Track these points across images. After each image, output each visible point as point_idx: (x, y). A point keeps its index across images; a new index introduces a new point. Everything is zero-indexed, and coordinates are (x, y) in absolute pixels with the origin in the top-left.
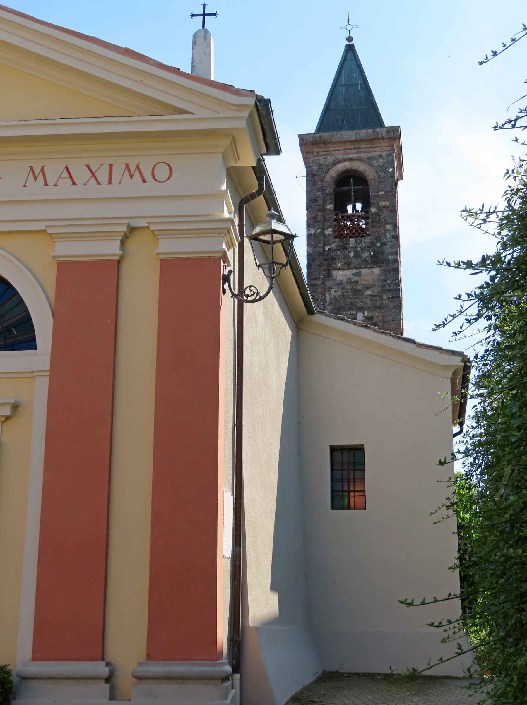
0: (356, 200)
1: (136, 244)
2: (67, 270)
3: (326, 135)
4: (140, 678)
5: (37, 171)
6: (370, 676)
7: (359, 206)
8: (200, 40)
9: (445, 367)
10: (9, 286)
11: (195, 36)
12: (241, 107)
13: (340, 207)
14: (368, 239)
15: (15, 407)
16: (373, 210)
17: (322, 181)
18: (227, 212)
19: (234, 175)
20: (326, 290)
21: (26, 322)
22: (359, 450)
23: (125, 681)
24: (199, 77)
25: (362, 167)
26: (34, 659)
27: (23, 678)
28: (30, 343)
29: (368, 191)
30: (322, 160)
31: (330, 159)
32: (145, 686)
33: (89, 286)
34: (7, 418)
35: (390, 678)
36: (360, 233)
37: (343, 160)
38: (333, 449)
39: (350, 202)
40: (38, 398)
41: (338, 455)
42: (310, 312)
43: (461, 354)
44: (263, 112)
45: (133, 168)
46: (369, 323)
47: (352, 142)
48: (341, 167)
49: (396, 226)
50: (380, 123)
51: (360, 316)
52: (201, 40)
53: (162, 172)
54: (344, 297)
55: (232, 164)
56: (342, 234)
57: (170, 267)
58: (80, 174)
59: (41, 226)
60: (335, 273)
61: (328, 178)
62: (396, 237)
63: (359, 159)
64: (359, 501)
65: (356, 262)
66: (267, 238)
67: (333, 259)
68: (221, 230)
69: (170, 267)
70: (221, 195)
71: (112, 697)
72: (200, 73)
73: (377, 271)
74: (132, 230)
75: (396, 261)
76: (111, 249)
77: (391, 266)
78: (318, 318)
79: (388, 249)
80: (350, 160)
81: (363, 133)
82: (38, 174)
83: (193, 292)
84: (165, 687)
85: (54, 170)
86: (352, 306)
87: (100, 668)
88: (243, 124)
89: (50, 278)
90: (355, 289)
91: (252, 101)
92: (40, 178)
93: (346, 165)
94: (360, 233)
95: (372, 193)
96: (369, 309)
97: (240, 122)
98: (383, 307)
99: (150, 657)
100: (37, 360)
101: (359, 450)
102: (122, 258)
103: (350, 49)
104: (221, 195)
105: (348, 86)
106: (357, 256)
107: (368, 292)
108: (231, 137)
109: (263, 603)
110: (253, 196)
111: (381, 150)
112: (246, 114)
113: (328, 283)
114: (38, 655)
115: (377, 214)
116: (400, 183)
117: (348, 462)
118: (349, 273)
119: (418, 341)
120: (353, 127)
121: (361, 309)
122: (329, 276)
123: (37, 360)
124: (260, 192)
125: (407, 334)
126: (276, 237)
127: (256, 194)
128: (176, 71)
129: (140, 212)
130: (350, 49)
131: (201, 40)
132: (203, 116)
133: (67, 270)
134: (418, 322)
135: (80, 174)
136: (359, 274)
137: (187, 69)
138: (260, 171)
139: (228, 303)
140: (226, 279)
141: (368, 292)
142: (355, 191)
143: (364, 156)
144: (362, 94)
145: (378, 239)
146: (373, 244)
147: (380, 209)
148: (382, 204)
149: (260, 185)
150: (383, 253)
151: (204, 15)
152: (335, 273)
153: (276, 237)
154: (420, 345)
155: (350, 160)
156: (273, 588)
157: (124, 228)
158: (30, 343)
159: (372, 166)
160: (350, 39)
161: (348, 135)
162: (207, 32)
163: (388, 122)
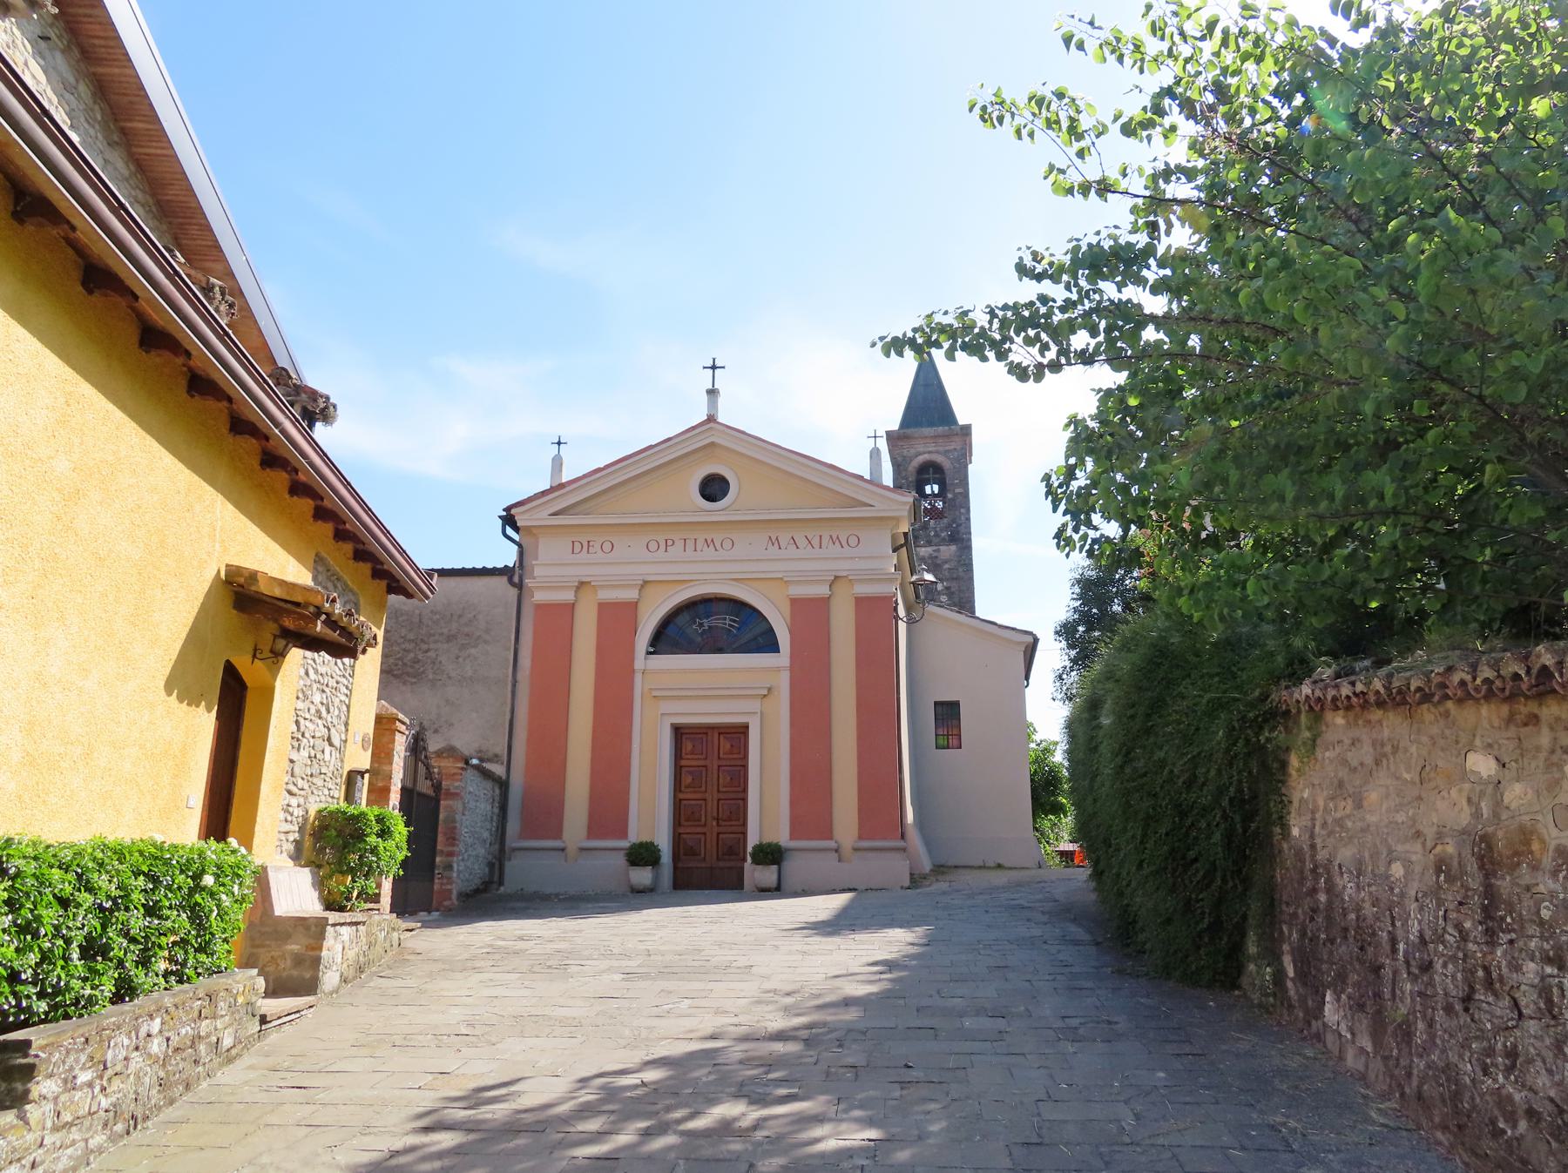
3: (909, 431)
4: (856, 849)
7: (936, 488)
15: (769, 689)
25: (939, 459)
30: (905, 452)
31: (913, 451)
32: (859, 854)
37: (924, 451)
38: (936, 703)
40: (783, 683)
43: (1030, 633)
48: (921, 459)
50: (955, 421)
53: (853, 541)
57: (862, 603)
58: (802, 542)
62: (968, 519)
65: (935, 540)
69: (862, 603)
73: (953, 548)
76: (823, 590)
79: (962, 529)
84: (871, 854)
85: (784, 539)
88: (906, 514)
93: (926, 457)
99: (860, 838)
100: (783, 658)
105: (926, 386)
106: (937, 535)
108: (897, 520)
111: (955, 444)
114: (793, 836)
117: (948, 713)
118: (930, 549)
120: (931, 424)
123: (783, 658)
128: (861, 478)
129: (843, 567)
133: (795, 602)
135: (802, 542)
137: (867, 477)
145: (954, 521)
146: (950, 525)
147: (956, 495)
154: (1001, 626)
161: (927, 431)
163: (962, 421)
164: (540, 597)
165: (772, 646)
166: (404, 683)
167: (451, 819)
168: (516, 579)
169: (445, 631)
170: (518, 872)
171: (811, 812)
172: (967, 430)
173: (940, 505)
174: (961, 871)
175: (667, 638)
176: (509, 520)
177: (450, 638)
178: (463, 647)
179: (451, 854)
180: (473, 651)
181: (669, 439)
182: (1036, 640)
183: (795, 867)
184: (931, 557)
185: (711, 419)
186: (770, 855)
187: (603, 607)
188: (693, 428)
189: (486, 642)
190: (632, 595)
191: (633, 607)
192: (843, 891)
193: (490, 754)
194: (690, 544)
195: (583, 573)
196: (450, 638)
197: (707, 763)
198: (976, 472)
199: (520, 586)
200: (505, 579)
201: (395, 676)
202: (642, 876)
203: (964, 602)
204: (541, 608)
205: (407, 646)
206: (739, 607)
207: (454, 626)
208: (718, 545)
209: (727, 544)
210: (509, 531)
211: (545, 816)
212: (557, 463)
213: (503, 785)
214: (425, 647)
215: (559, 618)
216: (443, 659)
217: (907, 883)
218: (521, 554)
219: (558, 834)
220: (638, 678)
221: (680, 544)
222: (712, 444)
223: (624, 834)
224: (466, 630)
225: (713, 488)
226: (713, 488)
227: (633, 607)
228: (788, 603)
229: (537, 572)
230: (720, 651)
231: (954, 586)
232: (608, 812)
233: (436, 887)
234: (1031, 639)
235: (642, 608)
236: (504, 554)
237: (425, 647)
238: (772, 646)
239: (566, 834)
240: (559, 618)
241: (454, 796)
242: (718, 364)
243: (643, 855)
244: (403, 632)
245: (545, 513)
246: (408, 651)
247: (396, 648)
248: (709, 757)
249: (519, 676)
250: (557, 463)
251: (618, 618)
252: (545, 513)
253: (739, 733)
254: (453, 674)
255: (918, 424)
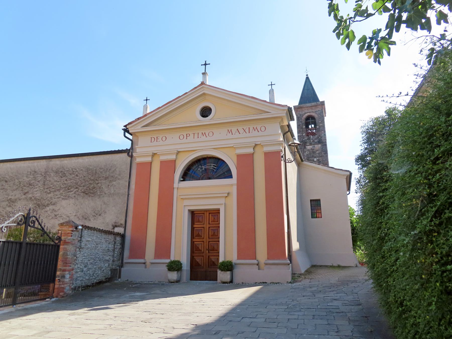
0: (312, 124)
1: (257, 149)
2: (239, 157)
3: (301, 105)
4: (266, 264)
5: (230, 131)
6: (326, 266)
7: (313, 126)
8: (271, 92)
9: (344, 175)
10: (224, 161)
11: (270, 91)
12: (284, 110)
13: (307, 127)
14: (316, 136)
15: (228, 194)
16: (318, 127)
17: (301, 119)
18: (281, 139)
19: (282, 127)
20: (304, 152)
21: (229, 171)
22: (319, 201)
23: (262, 265)
24: (272, 103)
25: (313, 114)
26: (238, 259)
27: (236, 264)
28: (230, 176)
29: (315, 122)
31: (303, 112)
32: (267, 266)
33: (246, 161)
34: (226, 197)
35: (332, 267)
36: (313, 134)
38: (311, 201)
39: (310, 124)
41: (312, 202)
42: (302, 161)
43: (348, 171)
44: (290, 111)
45: (255, 128)
46: (319, 162)
47: (310, 107)
48: (307, 115)
49: (325, 131)
51: (315, 160)
52: (271, 92)
53: (263, 129)
54: (310, 154)
55: (282, 124)
56: (308, 134)
58: (241, 131)
59: (232, 145)
60: (307, 147)
61: (303, 119)
62: (325, 135)
63: (313, 112)
64: (320, 215)
65: (313, 143)
66: (293, 145)
67: (306, 143)
68: (280, 144)
69: (267, 155)
70: (280, 134)
71: (259, 269)
72: (273, 102)
73: (320, 145)
74: (256, 145)
75: (326, 142)
76: (251, 150)
77: (324, 144)
78: (305, 162)
79: (323, 138)
80: (310, 112)
81: (313, 104)
82: (230, 132)
83: (274, 161)
85: (234, 130)
86: (313, 157)
87: (255, 262)
88: (285, 115)
89: (235, 159)
90: (313, 151)
91: (287, 108)
92: (231, 132)
93: (309, 114)
94: (313, 134)
95: (317, 122)
96: (318, 157)
97: (284, 114)
98: (323, 158)
99: (268, 259)
100: (234, 181)
101: (319, 201)
102: (254, 153)
103: (307, 78)
104: (280, 134)
105: (308, 90)
106: (313, 141)
107: (317, 152)
108: (281, 118)
109: (296, 246)
110: (287, 132)
111: (319, 108)
112: (285, 112)
113: (305, 150)
114: (239, 258)
115: (319, 128)
116: (325, 118)
117: (316, 205)
118: (311, 147)
119: (335, 168)
120: (310, 102)
121: (315, 157)
122: (305, 148)
123: (234, 181)
124: (289, 131)
125: (330, 166)
126: (295, 145)
127: (287, 131)
128: (265, 101)
129: (258, 140)
130: (307, 78)
131: (271, 92)
132: (274, 113)
133: (239, 157)
134: (334, 160)
135: (241, 131)
136: (314, 147)
137: (268, 101)
138: (289, 126)
139: (283, 163)
140: (282, 157)
141: (317, 152)
142: (312, 122)
143: (314, 111)
144: (312, 92)
146: (318, 137)
147: (320, 126)
148: (321, 125)
149: (289, 129)
150: (321, 140)
151: (272, 85)
152: (307, 147)
153: (295, 145)
154: (336, 169)
155: (310, 112)
156: (298, 241)
157: (254, 145)
158: (230, 176)
159: (316, 114)
160: (307, 75)
162: (273, 90)
163: (321, 100)
164: (138, 160)
165: (230, 176)
166: (89, 196)
167: (65, 254)
168: (130, 154)
169: (104, 175)
170: (128, 272)
171: (247, 247)
172: (323, 103)
173: (314, 131)
174: (321, 271)
175: (187, 175)
176: (126, 130)
177: (106, 178)
178: (111, 181)
179: (64, 270)
180: (114, 183)
181: (186, 93)
182: (351, 174)
183: (240, 273)
184: (312, 149)
185: (203, 83)
186: (228, 267)
187: (162, 162)
188: (196, 88)
189: (119, 179)
190: (173, 157)
191: (174, 162)
192: (255, 284)
193: (119, 224)
194: (196, 136)
195: (154, 150)
196: (106, 178)
197: (204, 226)
198: (327, 120)
199: (132, 156)
200: (126, 154)
201: (86, 194)
202: (173, 276)
203: (325, 162)
204: (140, 164)
205: (91, 182)
206: (218, 161)
207: (108, 173)
208: (207, 135)
209: (211, 134)
210: (127, 134)
211: (138, 251)
212: (145, 107)
213: (123, 236)
214: (97, 182)
215: (146, 167)
216: (103, 187)
217: (290, 279)
218: (132, 144)
219: (143, 256)
220: (175, 191)
221: (192, 136)
222: (204, 94)
223: (169, 257)
224: (112, 175)
225: (206, 112)
226: (206, 112)
227: (174, 162)
228: (236, 158)
229: (138, 150)
230: (209, 178)
231: (321, 159)
232: (163, 248)
233: (56, 286)
234: (348, 173)
235: (177, 162)
236: (127, 145)
237: (97, 182)
238: (230, 176)
239: (146, 257)
240: (146, 167)
241: (66, 243)
242: (207, 63)
243: (175, 266)
244: (90, 176)
245: (139, 127)
246: (91, 184)
247: (87, 183)
248: (204, 223)
249: (130, 193)
250: (145, 107)
251: (168, 167)
252: (139, 127)
253: (217, 212)
254: (107, 192)
255: (305, 103)
